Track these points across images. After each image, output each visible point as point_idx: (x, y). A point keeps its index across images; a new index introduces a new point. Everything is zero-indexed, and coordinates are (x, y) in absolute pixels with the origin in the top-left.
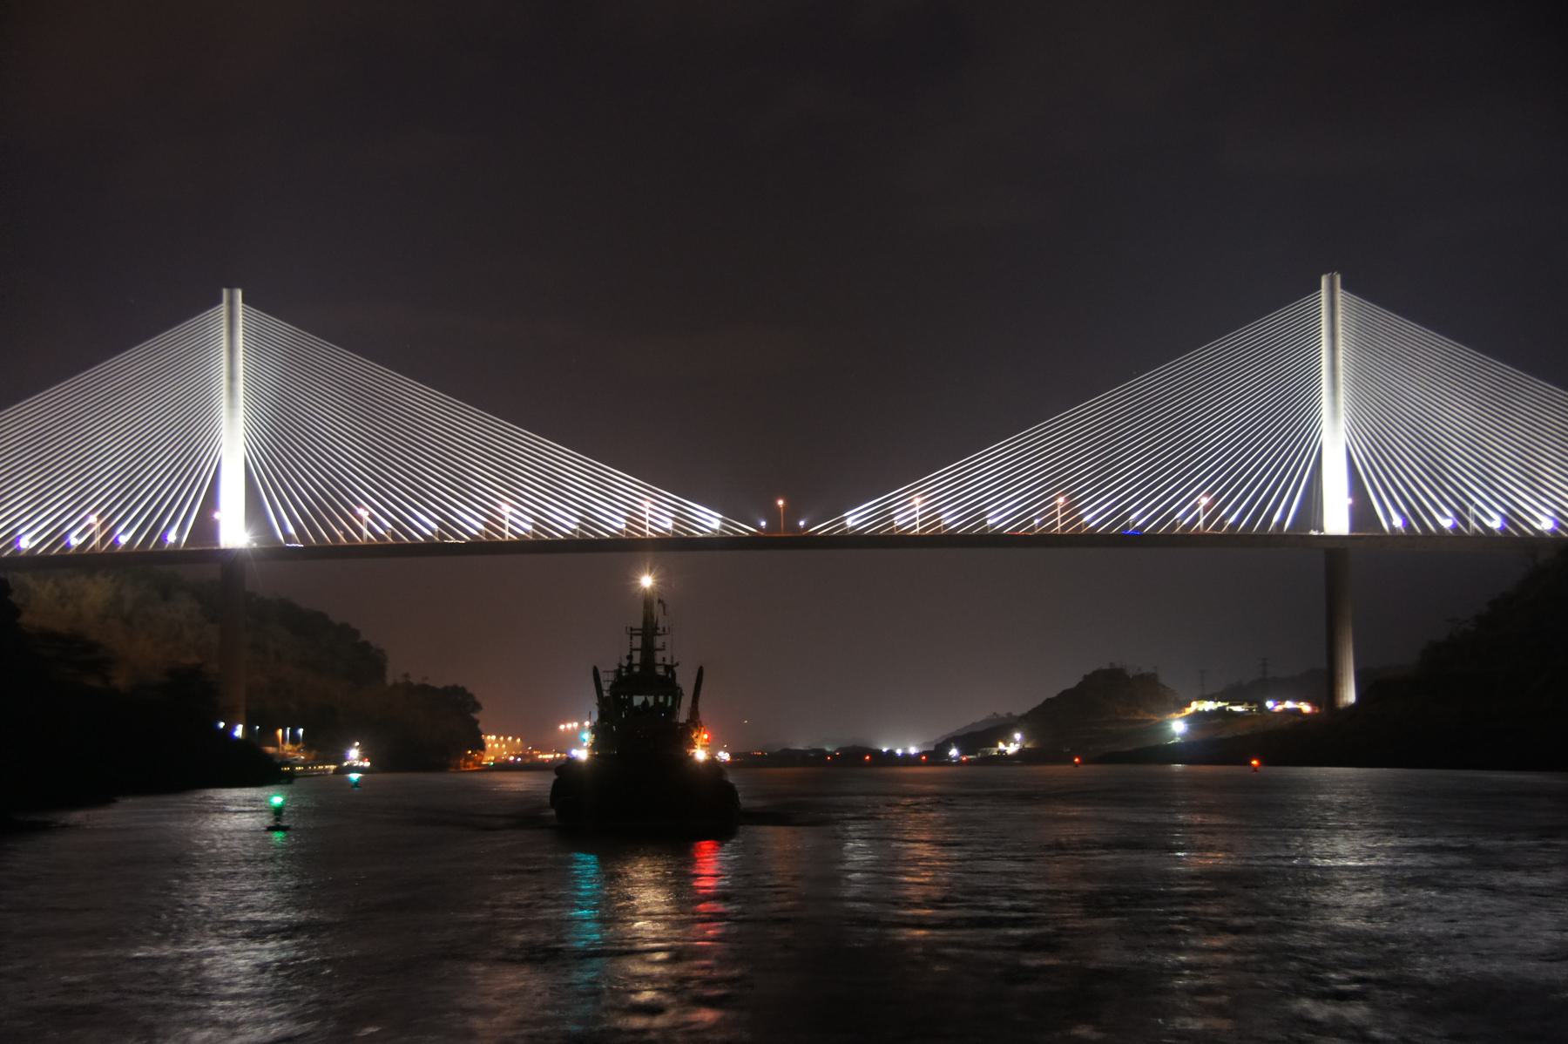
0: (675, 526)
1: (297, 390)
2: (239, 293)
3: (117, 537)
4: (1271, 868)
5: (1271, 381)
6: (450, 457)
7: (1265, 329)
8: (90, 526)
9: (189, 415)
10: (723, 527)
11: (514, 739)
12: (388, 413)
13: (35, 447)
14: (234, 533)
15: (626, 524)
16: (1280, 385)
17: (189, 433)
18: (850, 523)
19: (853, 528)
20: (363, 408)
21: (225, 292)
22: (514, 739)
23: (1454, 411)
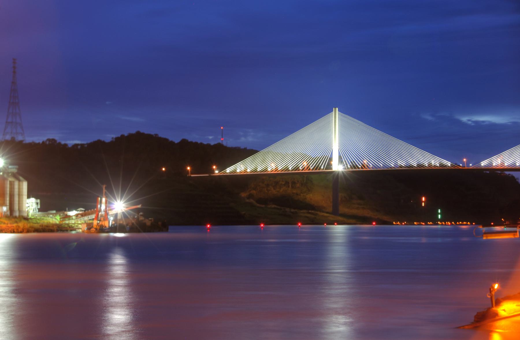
0: (428, 166)
1: (383, 147)
2: (337, 109)
3: (310, 168)
4: (506, 229)
5: (378, 151)
6: (392, 156)
7: (371, 147)
8: (304, 165)
9: (514, 152)
10: (451, 166)
11: (404, 223)
12: (389, 149)
13: (312, 150)
14: (337, 167)
15: (361, 166)
16: (352, 151)
17: (327, 149)
18: (482, 165)
19: (495, 166)
20: (378, 150)
21: (334, 109)
22: (404, 223)
23: (518, 156)
